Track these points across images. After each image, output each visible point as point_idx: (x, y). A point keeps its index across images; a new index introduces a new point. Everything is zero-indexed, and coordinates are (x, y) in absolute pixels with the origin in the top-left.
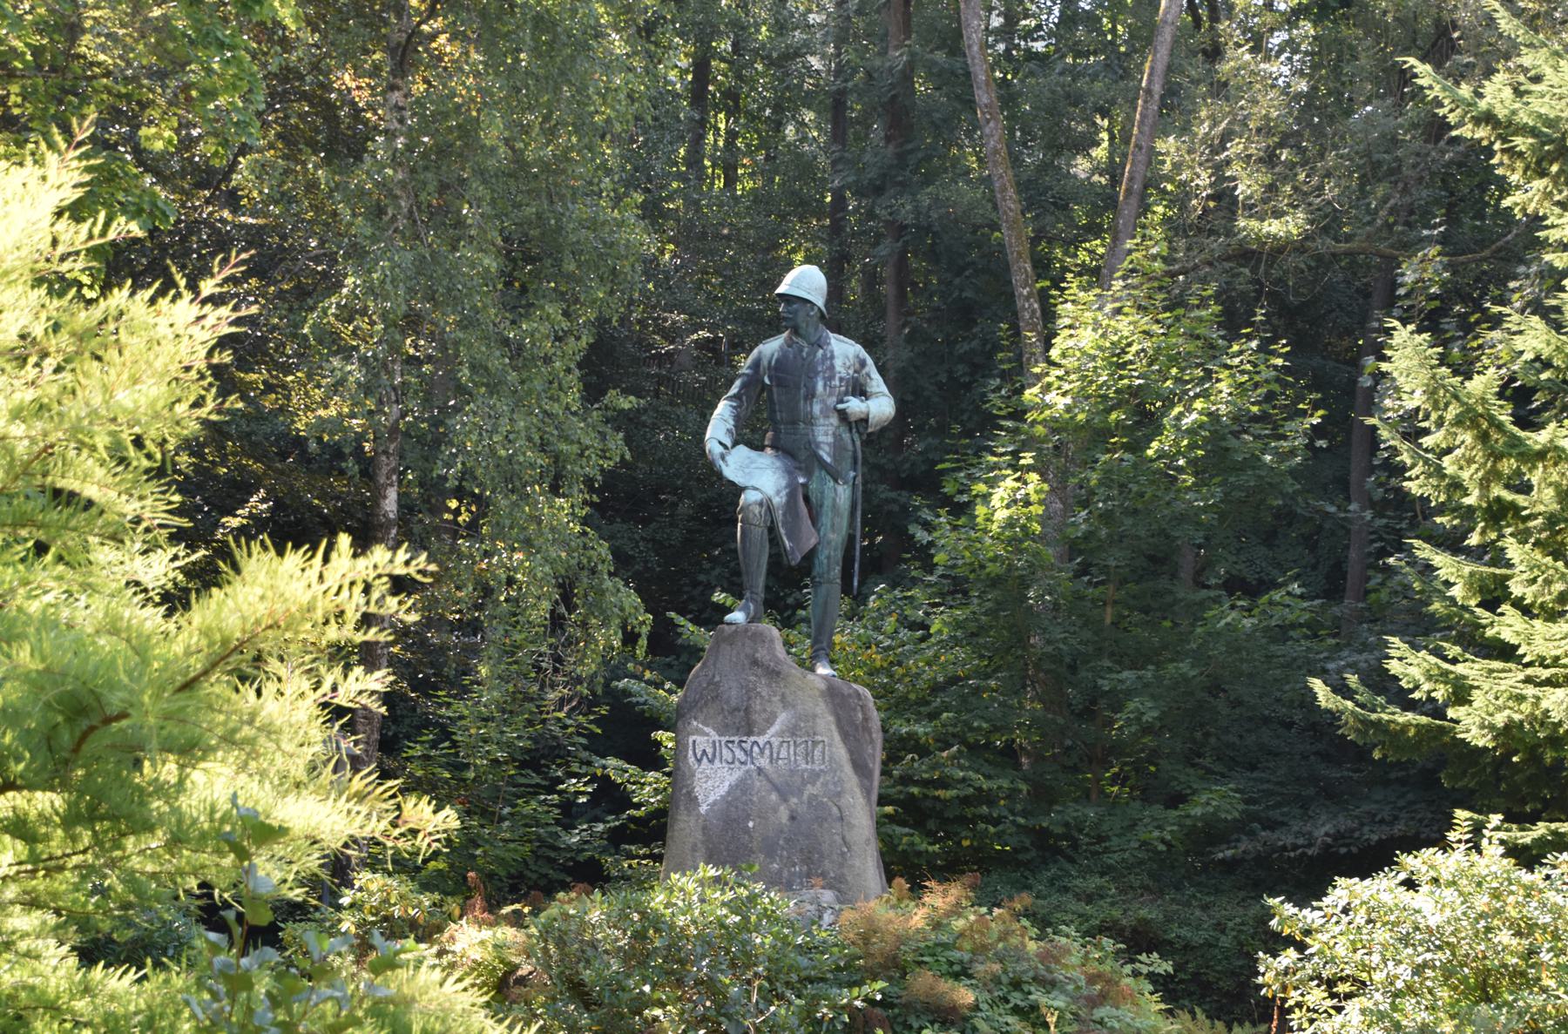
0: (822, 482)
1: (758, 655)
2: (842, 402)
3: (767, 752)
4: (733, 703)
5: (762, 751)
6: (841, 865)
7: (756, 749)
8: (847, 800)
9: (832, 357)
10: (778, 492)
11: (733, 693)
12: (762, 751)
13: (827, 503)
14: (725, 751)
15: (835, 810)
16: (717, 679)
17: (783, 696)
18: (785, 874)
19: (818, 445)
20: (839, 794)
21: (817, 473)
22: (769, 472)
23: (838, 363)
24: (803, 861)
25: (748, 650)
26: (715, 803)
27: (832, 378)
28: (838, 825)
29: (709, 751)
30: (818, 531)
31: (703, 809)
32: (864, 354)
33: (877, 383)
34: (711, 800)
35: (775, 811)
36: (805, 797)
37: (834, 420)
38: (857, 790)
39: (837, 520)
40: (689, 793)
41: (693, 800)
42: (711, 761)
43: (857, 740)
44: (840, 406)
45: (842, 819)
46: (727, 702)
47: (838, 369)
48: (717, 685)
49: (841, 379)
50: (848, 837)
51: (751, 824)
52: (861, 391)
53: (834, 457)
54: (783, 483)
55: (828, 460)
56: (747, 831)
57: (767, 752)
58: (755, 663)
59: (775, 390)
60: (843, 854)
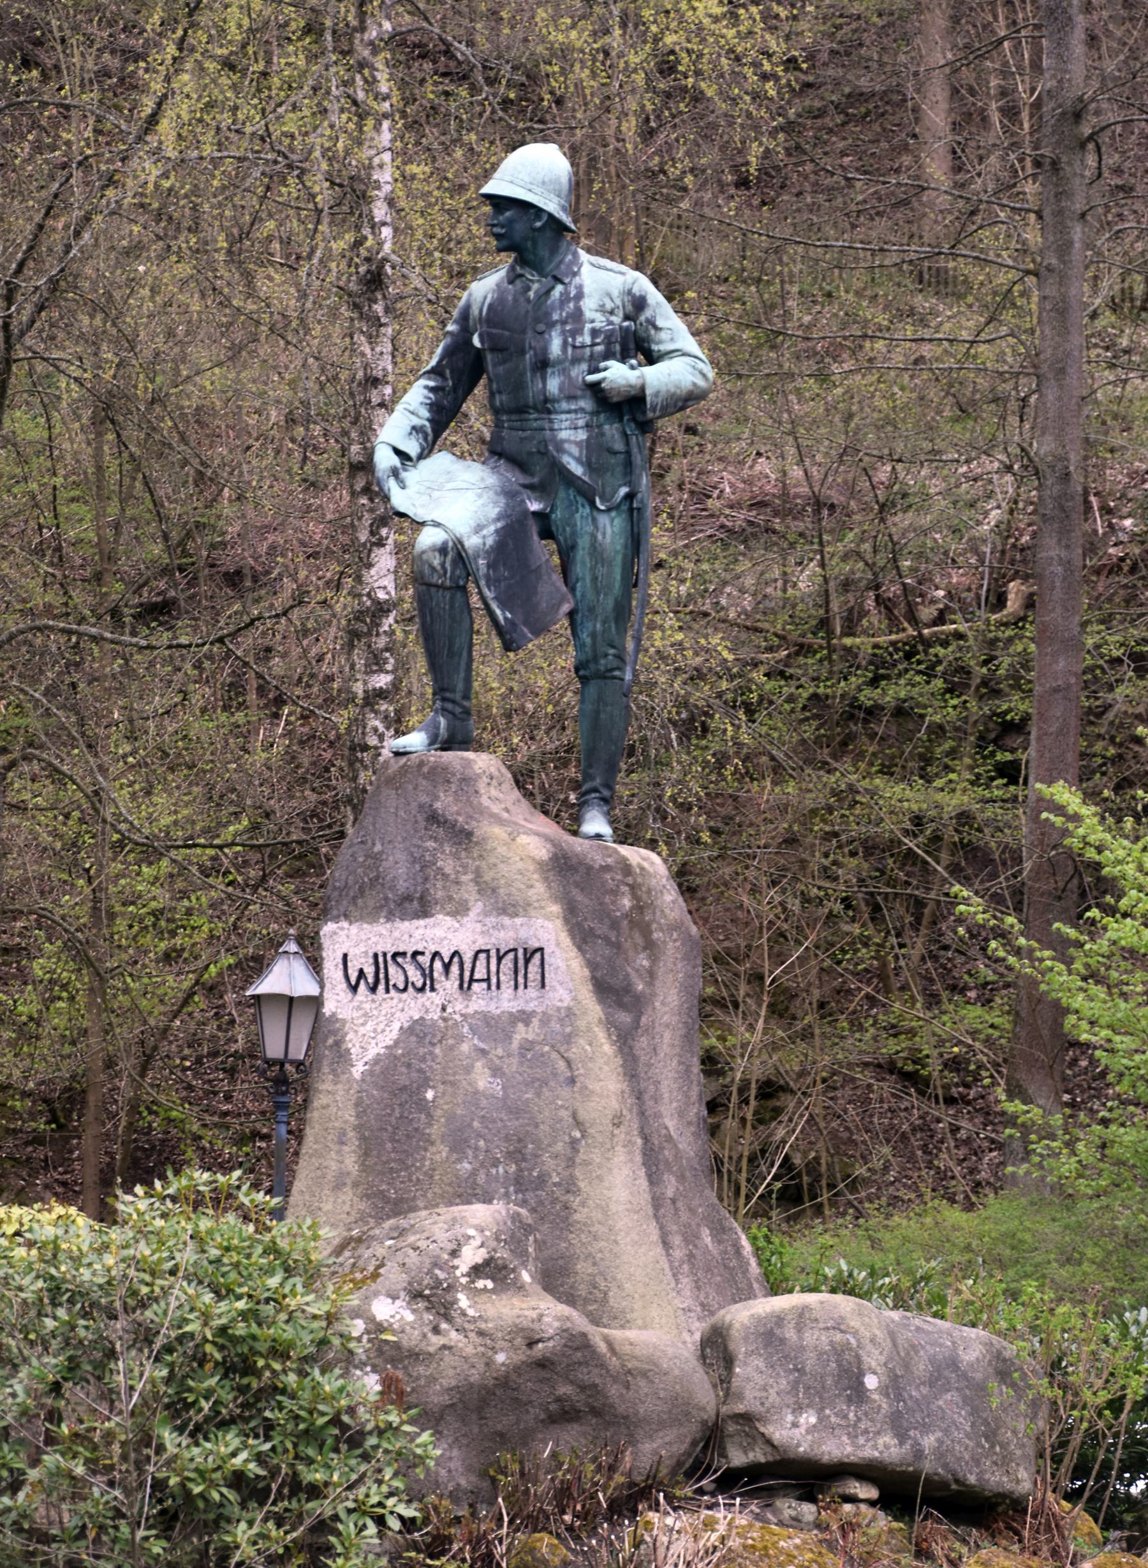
0: (572, 507)
1: (438, 805)
2: (597, 370)
3: (455, 969)
4: (402, 886)
5: (447, 967)
6: (571, 1163)
7: (438, 965)
8: (579, 1048)
9: (580, 296)
10: (478, 529)
11: (398, 869)
12: (447, 967)
13: (583, 543)
14: (392, 969)
15: (562, 1064)
16: (378, 848)
17: (478, 873)
18: (481, 1178)
19: (560, 446)
20: (568, 1039)
21: (562, 494)
22: (471, 495)
23: (589, 306)
24: (510, 1155)
25: (424, 799)
26: (377, 1060)
27: (578, 331)
28: (565, 1092)
29: (369, 971)
30: (573, 590)
31: (358, 1070)
32: (643, 284)
33: (671, 327)
34: (373, 1052)
35: (468, 1070)
36: (515, 1044)
37: (586, 404)
38: (601, 1034)
39: (601, 571)
40: (337, 1044)
41: (342, 1057)
42: (373, 989)
43: (618, 946)
44: (592, 378)
45: (572, 1081)
46: (392, 888)
47: (588, 314)
48: (377, 858)
49: (595, 333)
50: (582, 1115)
51: (430, 1095)
52: (638, 345)
53: (589, 465)
54: (494, 512)
55: (577, 470)
56: (423, 1106)
57: (455, 969)
58: (434, 818)
59: (489, 357)
60: (574, 1143)
